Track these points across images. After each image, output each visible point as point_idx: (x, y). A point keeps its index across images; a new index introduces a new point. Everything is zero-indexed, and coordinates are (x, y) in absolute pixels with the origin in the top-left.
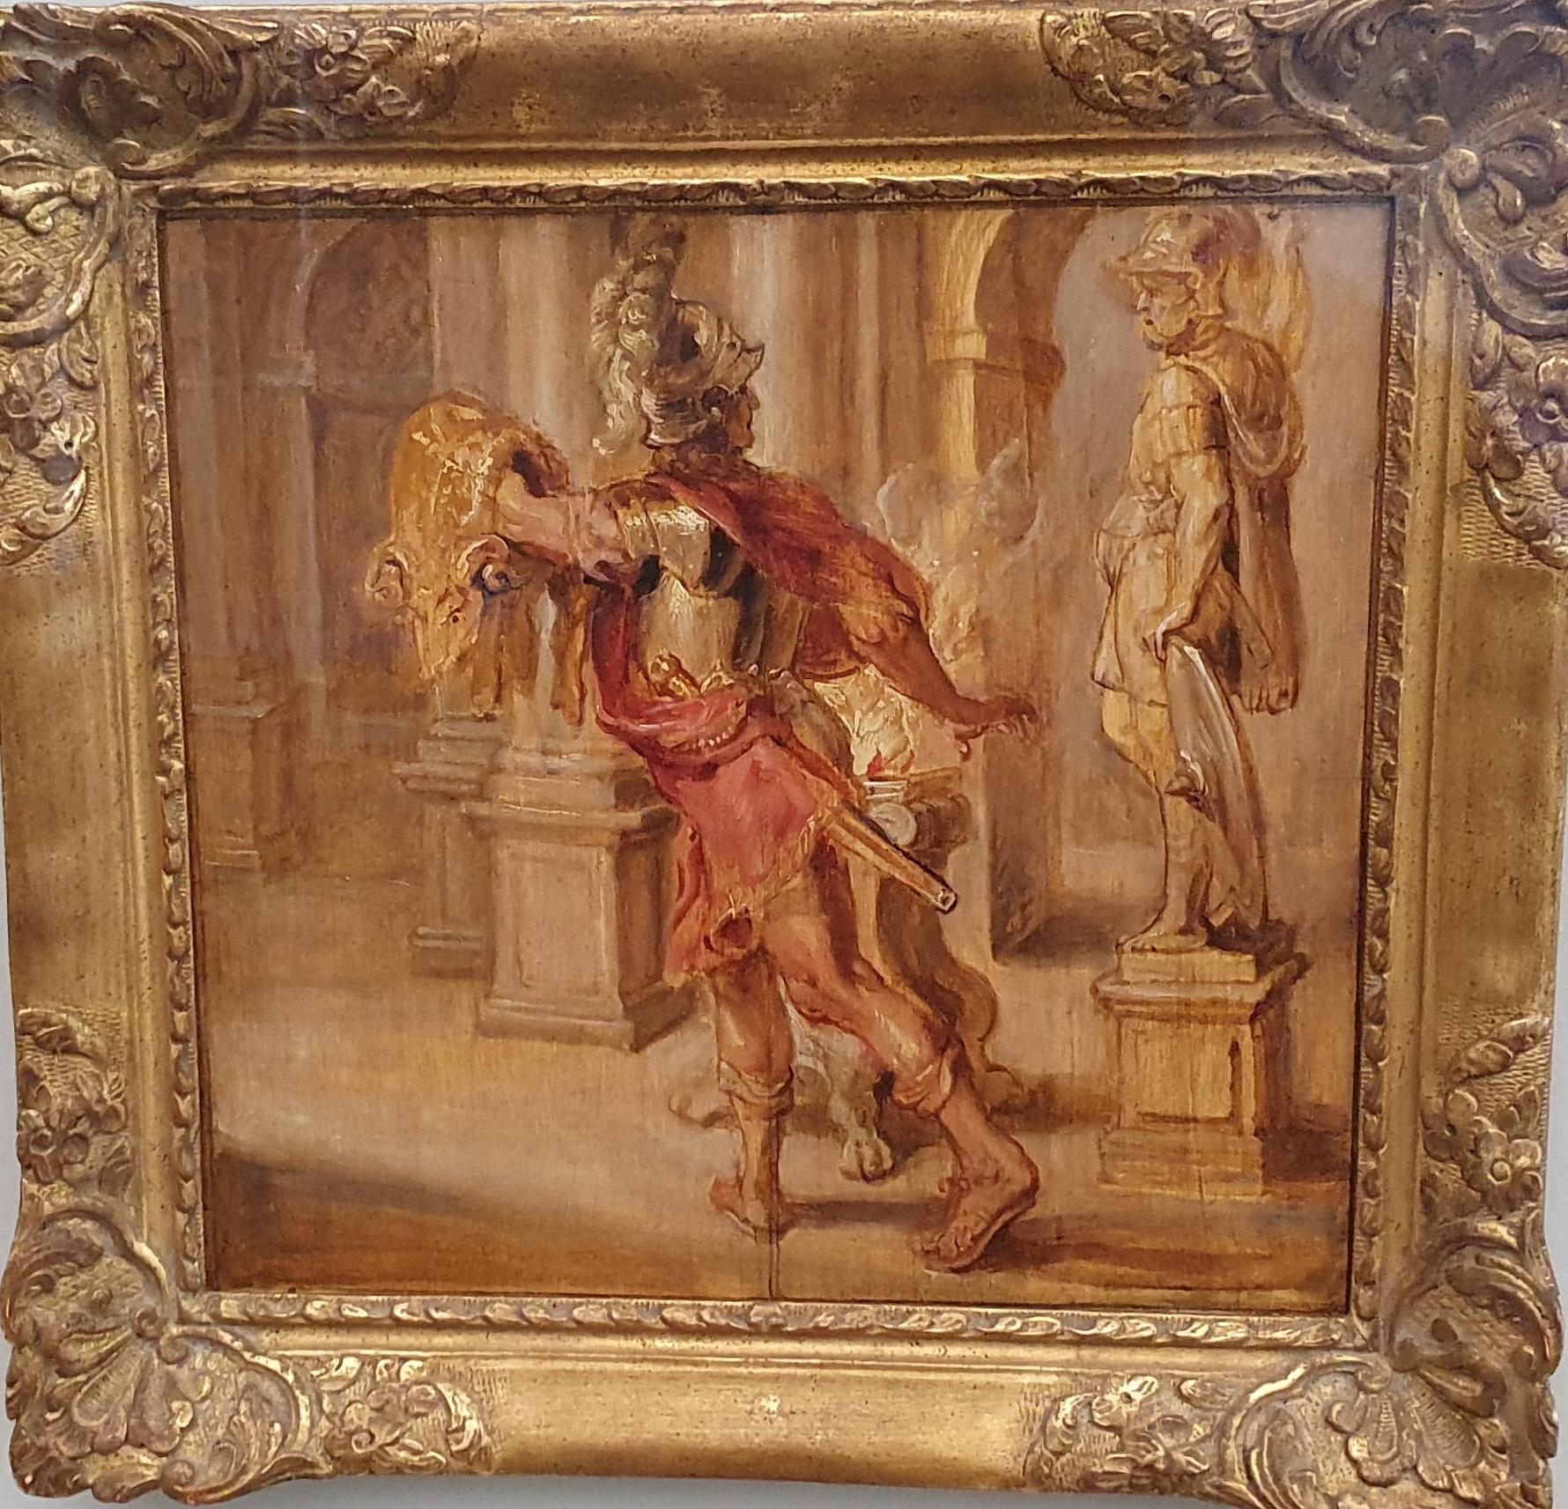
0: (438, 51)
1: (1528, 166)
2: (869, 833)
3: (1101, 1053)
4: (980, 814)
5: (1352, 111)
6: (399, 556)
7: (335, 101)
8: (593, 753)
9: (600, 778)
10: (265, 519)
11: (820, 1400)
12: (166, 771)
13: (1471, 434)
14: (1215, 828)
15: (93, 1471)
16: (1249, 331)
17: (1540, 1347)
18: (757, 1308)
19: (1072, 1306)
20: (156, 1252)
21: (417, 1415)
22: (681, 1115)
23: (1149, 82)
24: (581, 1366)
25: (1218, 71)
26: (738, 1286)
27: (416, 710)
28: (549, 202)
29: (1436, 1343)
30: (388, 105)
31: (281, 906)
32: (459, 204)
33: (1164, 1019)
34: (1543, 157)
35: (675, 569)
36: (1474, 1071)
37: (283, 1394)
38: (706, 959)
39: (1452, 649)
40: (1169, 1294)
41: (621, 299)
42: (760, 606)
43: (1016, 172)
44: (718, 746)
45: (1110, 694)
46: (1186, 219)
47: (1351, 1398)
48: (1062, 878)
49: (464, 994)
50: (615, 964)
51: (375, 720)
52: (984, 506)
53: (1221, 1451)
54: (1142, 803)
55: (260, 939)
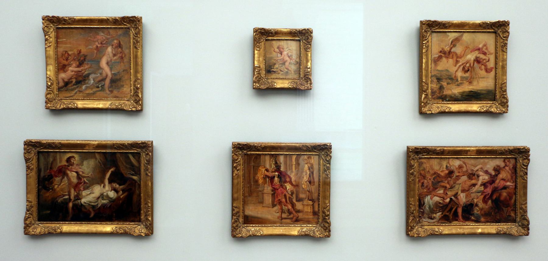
10: (250, 173)
31: (250, 198)
32: (263, 154)
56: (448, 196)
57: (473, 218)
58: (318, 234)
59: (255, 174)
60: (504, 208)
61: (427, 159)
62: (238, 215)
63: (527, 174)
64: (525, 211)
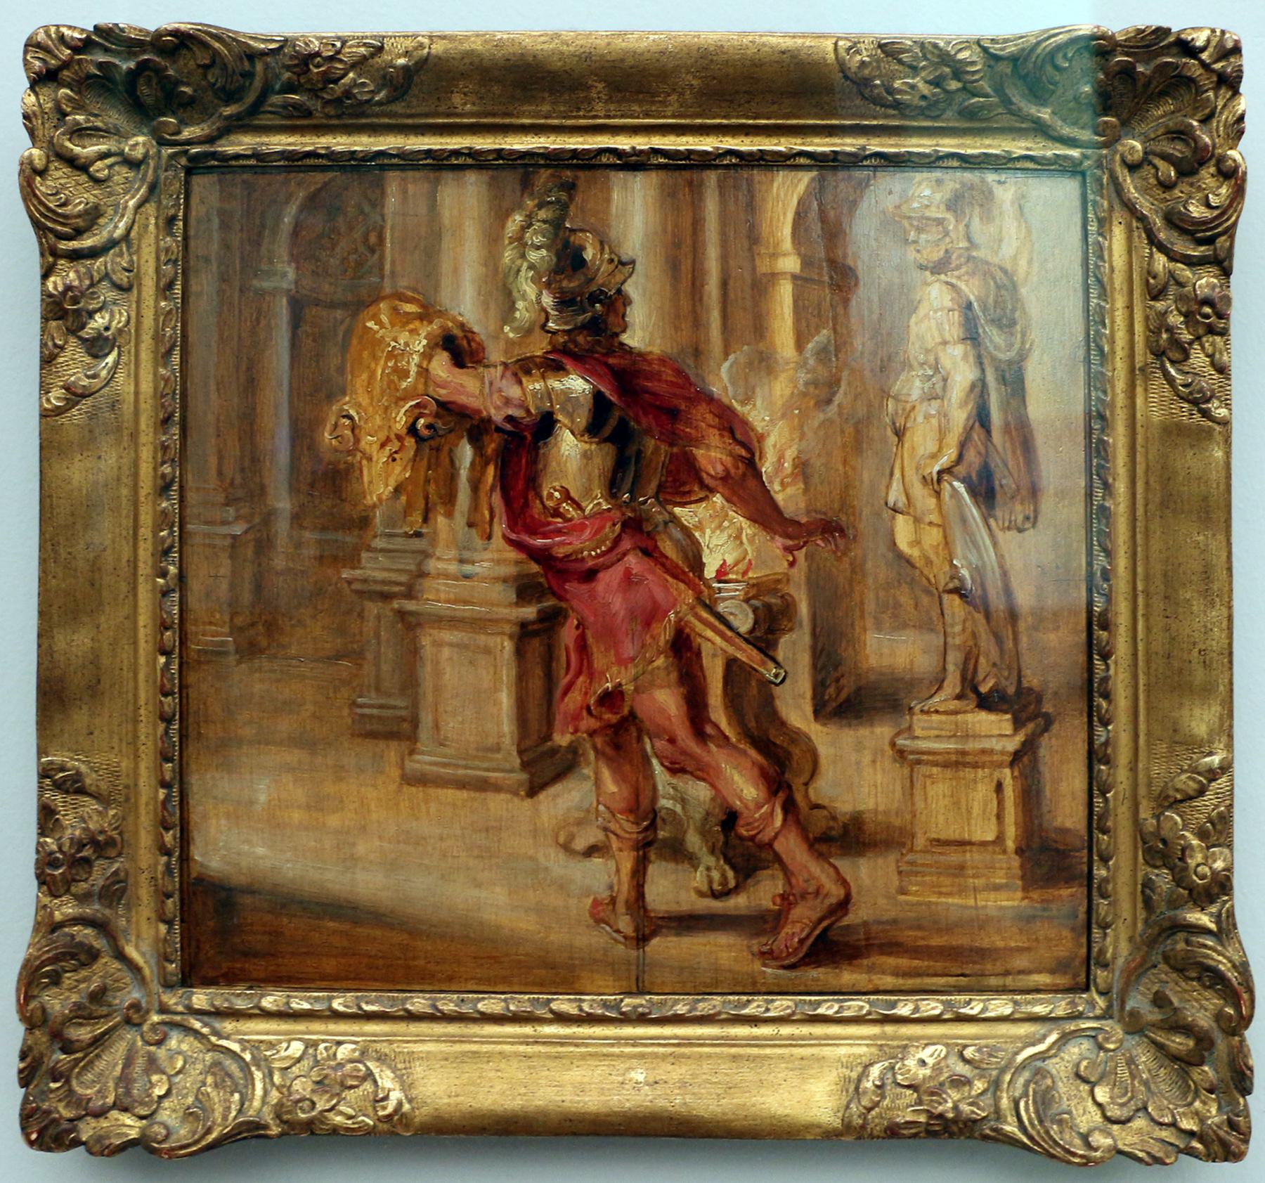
0: (399, 56)
1: (1177, 149)
2: (717, 623)
3: (898, 794)
4: (804, 609)
5: (1053, 113)
6: (352, 412)
7: (322, 90)
8: (498, 562)
9: (505, 581)
11: (677, 1072)
12: (164, 574)
13: (1150, 331)
14: (980, 617)
15: (87, 1130)
16: (989, 258)
17: (1237, 1007)
18: (627, 1001)
19: (876, 992)
20: (143, 954)
21: (352, 1087)
22: (567, 848)
23: (913, 87)
24: (485, 1048)
25: (959, 81)
26: (611, 983)
27: (361, 529)
28: (478, 161)
29: (1156, 1010)
30: (361, 93)
31: (251, 682)
32: (408, 161)
33: (945, 765)
34: (1188, 144)
35: (566, 421)
36: (1179, 797)
37: (242, 1070)
38: (588, 723)
39: (1147, 483)
40: (952, 980)
41: (528, 227)
42: (632, 450)
43: (818, 145)
44: (598, 556)
45: (900, 518)
46: (939, 182)
47: (1093, 1056)
48: (867, 657)
49: (392, 752)
50: (514, 728)
51: (330, 536)
52: (803, 377)
53: (997, 1100)
54: (925, 600)
55: (232, 707)
58: (1087, 1117)
59: (317, 389)
62: (99, 875)
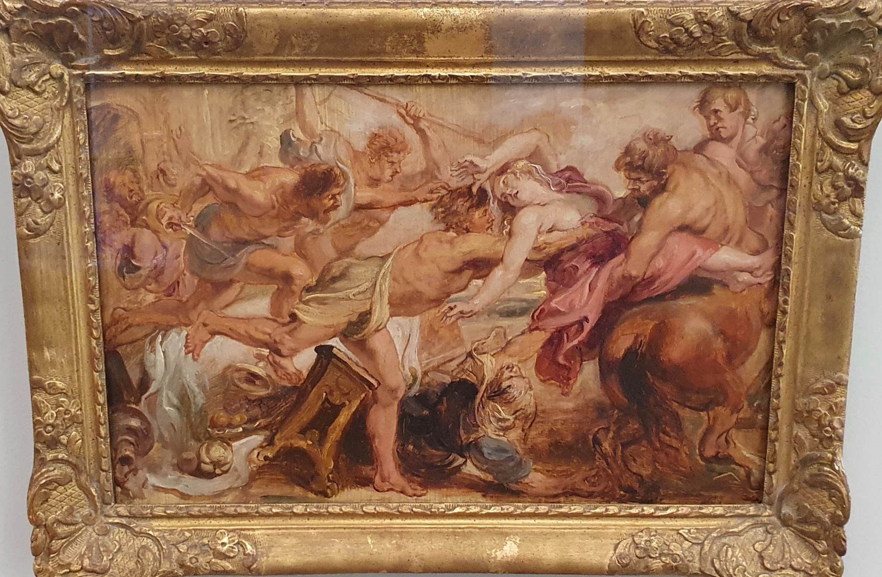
56: (304, 333)
57: (470, 469)
60: (686, 414)
61: (146, 93)
63: (858, 190)
64: (828, 438)
